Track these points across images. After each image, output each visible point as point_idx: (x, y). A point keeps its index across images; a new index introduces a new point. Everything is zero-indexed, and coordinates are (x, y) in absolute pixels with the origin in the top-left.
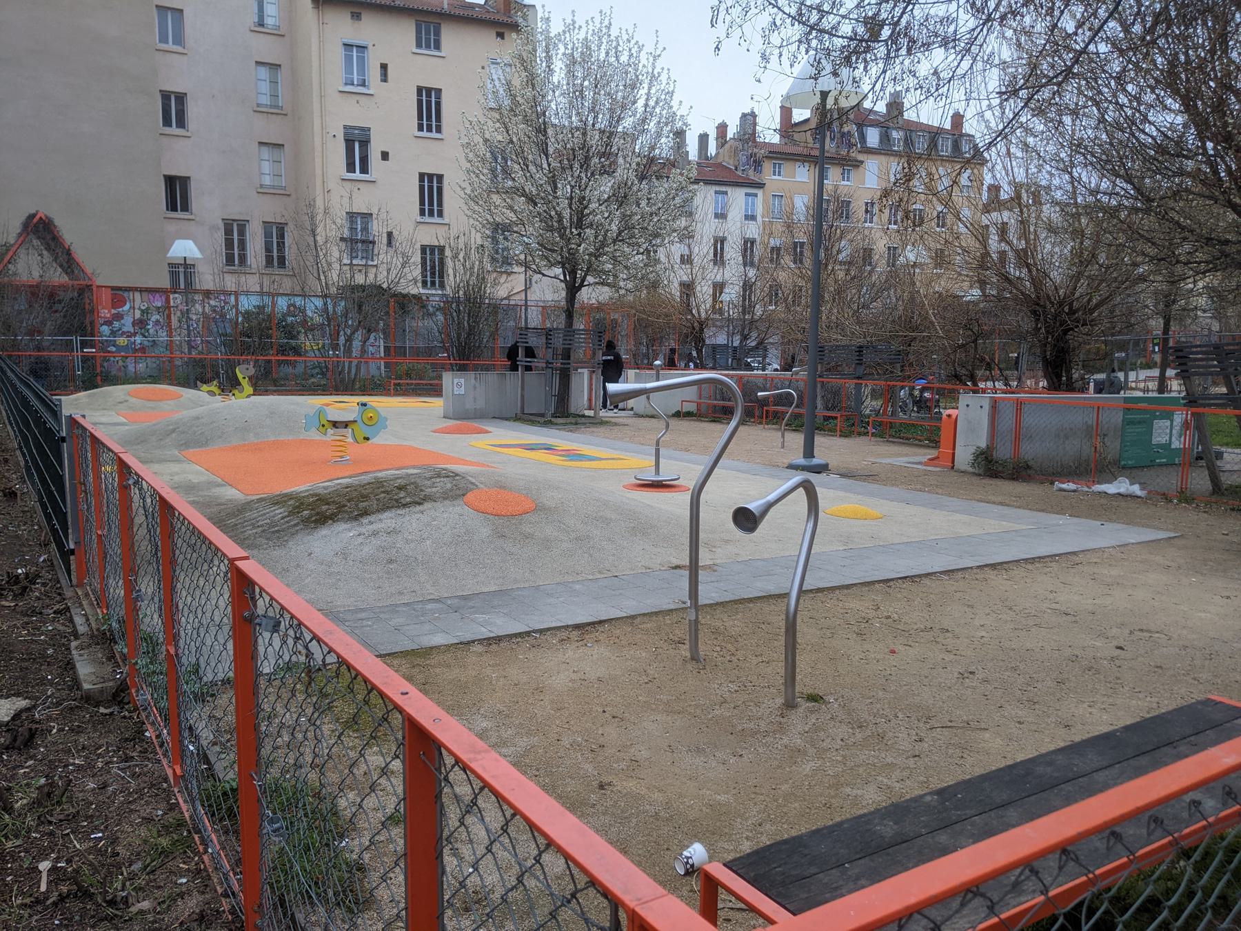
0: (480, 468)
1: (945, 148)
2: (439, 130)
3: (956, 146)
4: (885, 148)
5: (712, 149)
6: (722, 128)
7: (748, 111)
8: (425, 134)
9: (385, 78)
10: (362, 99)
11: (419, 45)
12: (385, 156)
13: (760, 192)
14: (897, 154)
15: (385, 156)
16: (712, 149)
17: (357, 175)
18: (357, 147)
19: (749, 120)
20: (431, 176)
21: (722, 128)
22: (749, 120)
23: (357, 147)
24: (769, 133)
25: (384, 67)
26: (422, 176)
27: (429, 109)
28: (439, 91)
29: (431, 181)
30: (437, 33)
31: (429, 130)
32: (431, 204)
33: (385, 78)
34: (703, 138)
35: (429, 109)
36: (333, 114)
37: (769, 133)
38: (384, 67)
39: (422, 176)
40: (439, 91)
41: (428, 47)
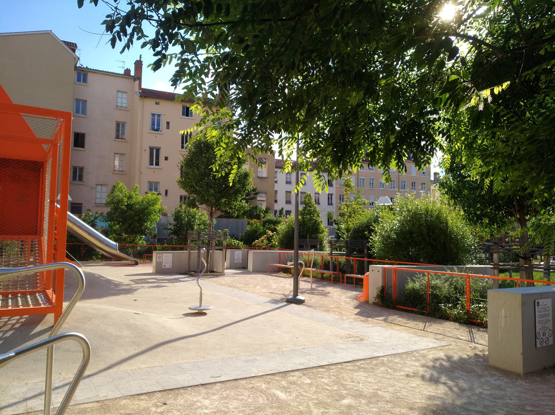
9: (168, 127)
12: (166, 159)
15: (166, 159)
17: (154, 166)
33: (168, 127)
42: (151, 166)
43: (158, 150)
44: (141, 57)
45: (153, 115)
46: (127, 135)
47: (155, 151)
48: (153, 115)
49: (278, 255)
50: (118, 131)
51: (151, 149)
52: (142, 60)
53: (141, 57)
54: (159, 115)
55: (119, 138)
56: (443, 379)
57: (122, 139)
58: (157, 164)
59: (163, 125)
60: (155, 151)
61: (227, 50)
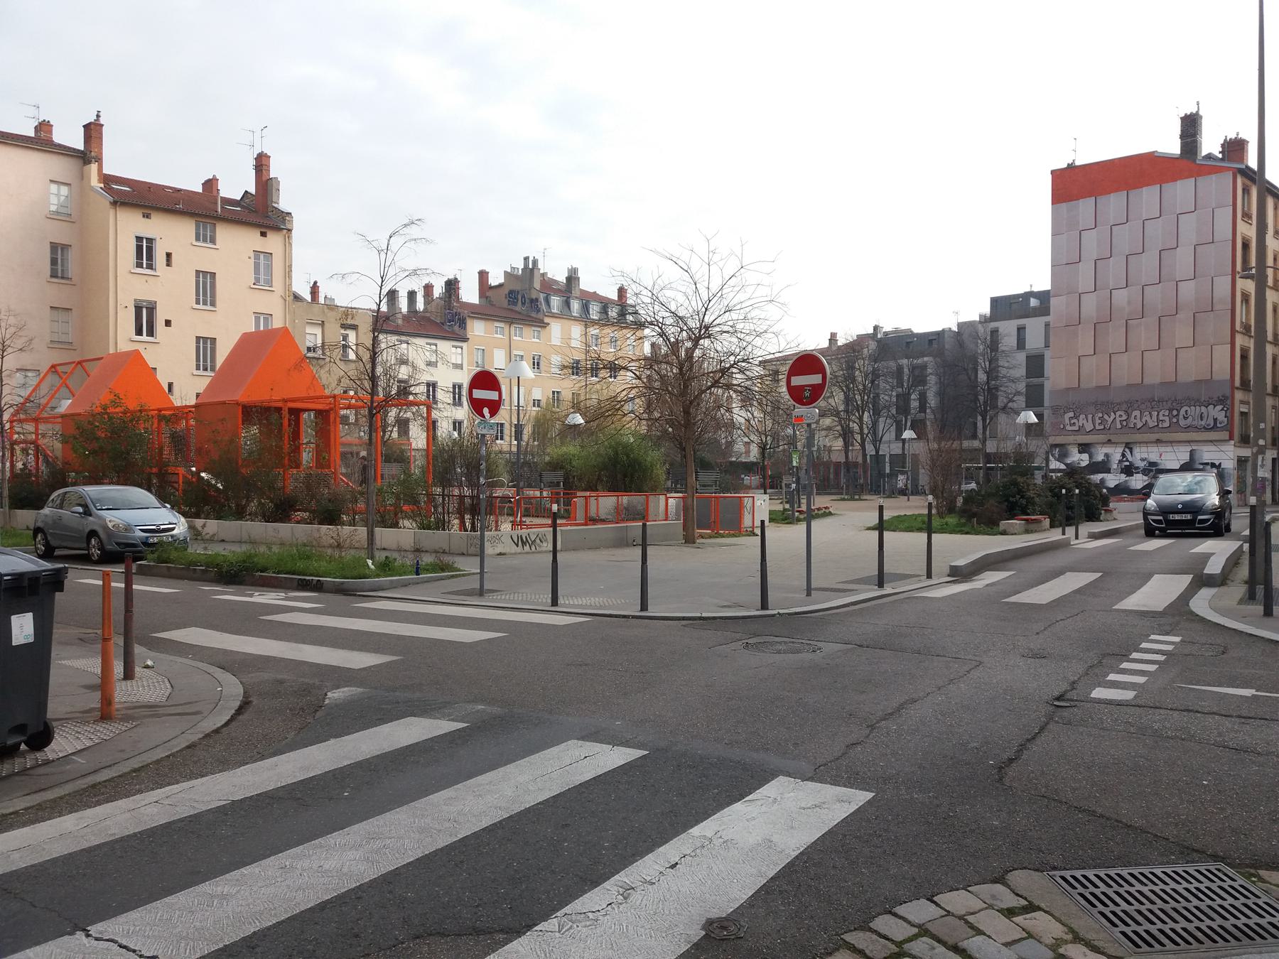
0: (244, 548)
1: (613, 313)
2: (213, 304)
3: (622, 314)
4: (566, 313)
5: (420, 305)
6: (428, 288)
7: (451, 277)
8: (201, 306)
9: (169, 264)
10: (151, 279)
11: (197, 239)
12: (168, 323)
13: (464, 345)
14: (575, 319)
15: (168, 323)
16: (420, 305)
17: (144, 338)
18: (145, 318)
19: (452, 285)
20: (205, 339)
21: (428, 288)
22: (452, 285)
23: (145, 318)
24: (469, 294)
25: (169, 255)
26: (198, 338)
27: (206, 287)
28: (213, 340)
29: (205, 343)
30: (214, 231)
31: (205, 303)
32: (205, 360)
33: (169, 264)
34: (412, 295)
35: (206, 287)
36: (128, 285)
37: (469, 294)
38: (169, 255)
39: (198, 338)
40: (213, 340)
41: (205, 241)
42: (139, 338)
43: (152, 309)
44: (98, 116)
45: (139, 239)
46: (73, 269)
47: (144, 311)
48: (139, 239)
49: (56, 312)
50: (54, 262)
51: (138, 309)
52: (102, 121)
53: (98, 116)
54: (150, 241)
55: (56, 277)
56: (805, 460)
57: (62, 278)
58: (151, 333)
59: (160, 258)
60: (144, 311)
61: (973, 485)
